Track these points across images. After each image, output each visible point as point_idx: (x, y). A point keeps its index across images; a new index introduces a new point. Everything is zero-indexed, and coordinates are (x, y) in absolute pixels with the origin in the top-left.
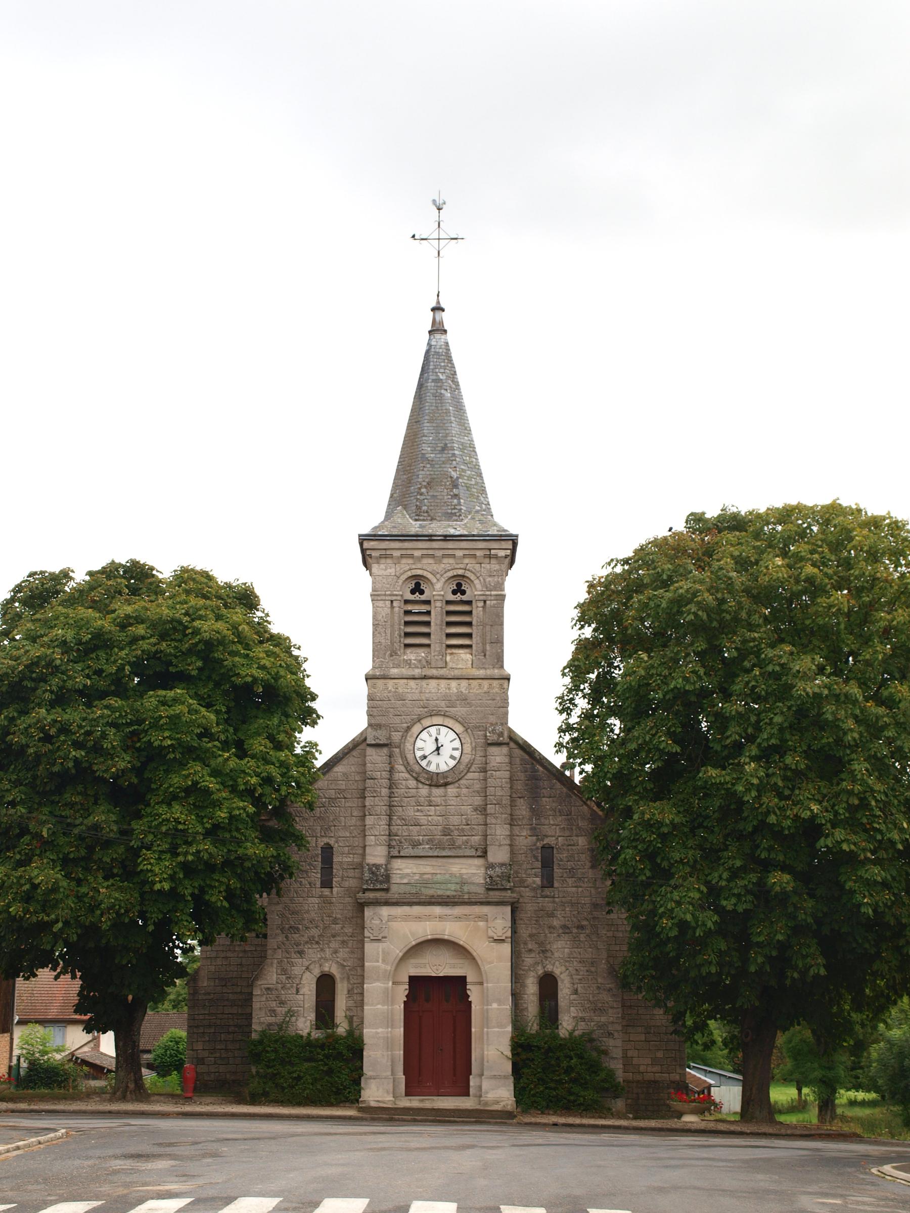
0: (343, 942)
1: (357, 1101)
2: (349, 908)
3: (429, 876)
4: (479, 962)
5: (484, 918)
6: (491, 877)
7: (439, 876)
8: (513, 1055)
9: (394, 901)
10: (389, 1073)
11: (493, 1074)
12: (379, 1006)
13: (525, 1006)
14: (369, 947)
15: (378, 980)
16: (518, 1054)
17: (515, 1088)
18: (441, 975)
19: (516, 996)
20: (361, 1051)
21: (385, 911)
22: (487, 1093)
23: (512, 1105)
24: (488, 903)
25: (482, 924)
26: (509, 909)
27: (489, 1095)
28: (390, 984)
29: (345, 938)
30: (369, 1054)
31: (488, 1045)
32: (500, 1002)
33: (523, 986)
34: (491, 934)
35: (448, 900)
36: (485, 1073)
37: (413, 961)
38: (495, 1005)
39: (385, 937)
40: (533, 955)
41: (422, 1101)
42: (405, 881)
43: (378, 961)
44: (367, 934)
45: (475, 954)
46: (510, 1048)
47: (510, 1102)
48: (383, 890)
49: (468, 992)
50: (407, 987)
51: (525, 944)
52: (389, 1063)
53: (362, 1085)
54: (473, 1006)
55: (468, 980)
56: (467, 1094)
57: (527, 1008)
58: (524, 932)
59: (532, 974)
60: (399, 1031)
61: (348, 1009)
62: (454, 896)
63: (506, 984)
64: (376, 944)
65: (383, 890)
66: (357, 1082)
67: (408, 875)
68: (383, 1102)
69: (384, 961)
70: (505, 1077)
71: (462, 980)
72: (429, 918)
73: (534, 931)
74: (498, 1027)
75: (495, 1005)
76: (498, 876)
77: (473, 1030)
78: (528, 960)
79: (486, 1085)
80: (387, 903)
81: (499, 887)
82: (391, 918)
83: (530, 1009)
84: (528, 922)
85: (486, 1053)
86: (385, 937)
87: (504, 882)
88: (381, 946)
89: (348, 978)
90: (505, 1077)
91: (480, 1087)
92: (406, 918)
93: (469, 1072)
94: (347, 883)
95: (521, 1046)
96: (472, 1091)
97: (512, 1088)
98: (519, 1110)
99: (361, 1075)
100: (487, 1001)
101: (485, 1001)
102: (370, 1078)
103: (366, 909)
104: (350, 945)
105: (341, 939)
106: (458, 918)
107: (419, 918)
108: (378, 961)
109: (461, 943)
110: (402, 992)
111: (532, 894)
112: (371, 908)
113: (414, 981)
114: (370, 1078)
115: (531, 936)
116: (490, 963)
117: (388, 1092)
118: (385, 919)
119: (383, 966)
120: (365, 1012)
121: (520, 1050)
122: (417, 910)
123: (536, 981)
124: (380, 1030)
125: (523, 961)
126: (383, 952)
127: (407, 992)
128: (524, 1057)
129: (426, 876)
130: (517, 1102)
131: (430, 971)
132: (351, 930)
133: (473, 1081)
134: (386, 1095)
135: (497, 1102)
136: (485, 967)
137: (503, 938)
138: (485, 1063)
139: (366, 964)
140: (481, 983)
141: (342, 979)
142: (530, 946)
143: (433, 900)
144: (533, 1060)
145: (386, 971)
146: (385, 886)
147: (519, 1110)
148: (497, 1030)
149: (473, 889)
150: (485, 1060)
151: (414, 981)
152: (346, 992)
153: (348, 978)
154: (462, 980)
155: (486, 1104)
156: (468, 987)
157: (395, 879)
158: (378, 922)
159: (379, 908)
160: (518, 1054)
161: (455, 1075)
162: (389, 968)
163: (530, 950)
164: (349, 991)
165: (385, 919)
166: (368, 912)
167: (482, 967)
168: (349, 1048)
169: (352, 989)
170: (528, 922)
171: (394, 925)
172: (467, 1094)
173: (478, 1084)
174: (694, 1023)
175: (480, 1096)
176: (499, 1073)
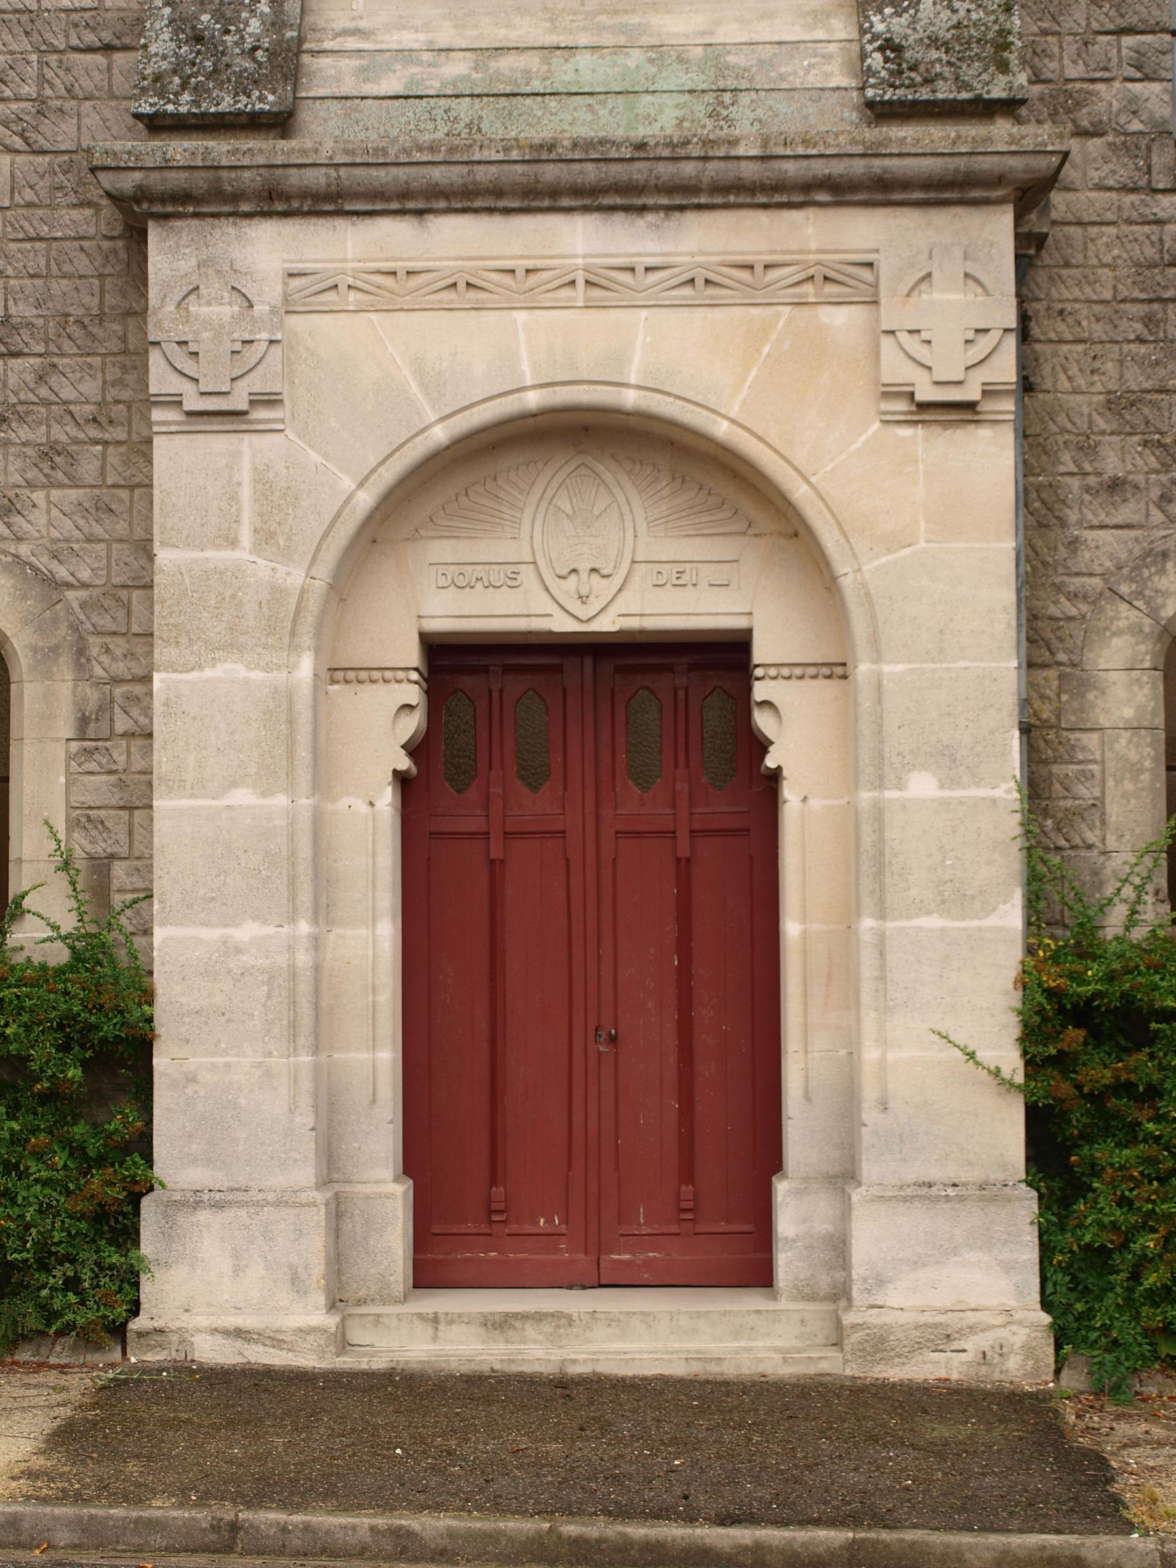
0: (50, 452)
1: (118, 1331)
2: (82, 264)
3: (532, 61)
4: (829, 539)
5: (854, 281)
6: (891, 47)
7: (584, 60)
8: (1033, 1065)
9: (316, 179)
10: (305, 1174)
11: (914, 1172)
12: (242, 797)
13: (1086, 792)
14: (181, 462)
15: (231, 646)
16: (1063, 1062)
17: (1046, 1250)
18: (607, 624)
19: (1044, 741)
20: (140, 1047)
21: (268, 250)
22: (881, 1282)
23: (1029, 1351)
24: (882, 191)
25: (842, 320)
26: (997, 229)
27: (893, 1297)
28: (306, 667)
29: (60, 434)
30: (178, 1066)
31: (885, 1011)
32: (950, 763)
33: (1077, 681)
34: (895, 368)
35: (638, 172)
36: (869, 1170)
37: (441, 550)
38: (923, 785)
39: (271, 401)
40: (1127, 512)
41: (501, 1324)
42: (390, 84)
43: (233, 543)
44: (161, 379)
45: (800, 493)
46: (1014, 1029)
47: (1019, 1337)
48: (254, 123)
49: (763, 721)
50: (413, 694)
51: (1087, 448)
52: (304, 1119)
53: (147, 1246)
54: (790, 793)
55: (761, 653)
56: (757, 1273)
57: (1098, 805)
58: (1078, 390)
59: (1126, 615)
60: (373, 941)
61: (84, 819)
62: (676, 150)
63: (993, 666)
64: (215, 446)
65: (254, 123)
66: (119, 1225)
67: (406, 55)
68: (275, 1341)
69: (265, 537)
70: (988, 1193)
71: (723, 659)
72: (526, 283)
73: (1136, 379)
74: (943, 906)
75: (923, 785)
76: (934, 42)
77: (791, 928)
78: (1103, 547)
79: (870, 1238)
80: (277, 201)
81: (944, 92)
82: (308, 291)
83: (1114, 811)
84: (1099, 330)
85: (870, 1054)
86: (271, 401)
87: (969, 72)
88: (246, 451)
89: (81, 651)
90: (988, 1193)
91: (838, 1248)
92: (392, 287)
93: (768, 1156)
94: (68, 127)
95: (1081, 1013)
96: (786, 1264)
97: (1030, 1254)
98: (1073, 1380)
99: (137, 1191)
100: (879, 757)
101: (862, 756)
102: (196, 1201)
103: (154, 234)
104: (88, 469)
105: (39, 435)
106: (702, 285)
107: (466, 288)
108: (233, 543)
109: (721, 430)
110: (384, 723)
111: (1124, 173)
112: (187, 229)
113: (451, 661)
114: (196, 1201)
115: (1115, 404)
116: (898, 541)
117: (296, 1282)
118: (268, 293)
119: (262, 569)
120: (163, 827)
121: (1074, 1036)
122: (456, 238)
123: (1147, 653)
124: (247, 932)
125: (1074, 544)
126: (263, 484)
127: (412, 724)
128: (1099, 1071)
129: (505, 64)
130: (1061, 1337)
131: (542, 603)
132: (90, 388)
133: (795, 1213)
134: (284, 1297)
135: (942, 1338)
136: (859, 568)
137: (971, 393)
138: (870, 1114)
139: (164, 557)
140: (837, 670)
141: (47, 656)
142: (1112, 463)
143: (550, 173)
144: (1154, 1093)
145: (277, 592)
146: (267, 101)
147: (1073, 1380)
148: (935, 922)
149: (789, 118)
150: (869, 1094)
151: (451, 661)
152: (65, 727)
153: (81, 651)
154: (723, 659)
155: (879, 1344)
156: (760, 691)
157: (329, 74)
158: (225, 311)
159: (228, 228)
160: (1063, 1062)
161: (688, 1174)
162: (295, 577)
163: (1115, 486)
164: (83, 722)
165: (268, 293)
166: (169, 255)
167: (842, 566)
168: (70, 1034)
169: (106, 706)
170: (1099, 330)
171: (319, 331)
172: (757, 1273)
173: (823, 1226)
174: (85, 1064)
175: (841, 1294)
176: (952, 1172)
